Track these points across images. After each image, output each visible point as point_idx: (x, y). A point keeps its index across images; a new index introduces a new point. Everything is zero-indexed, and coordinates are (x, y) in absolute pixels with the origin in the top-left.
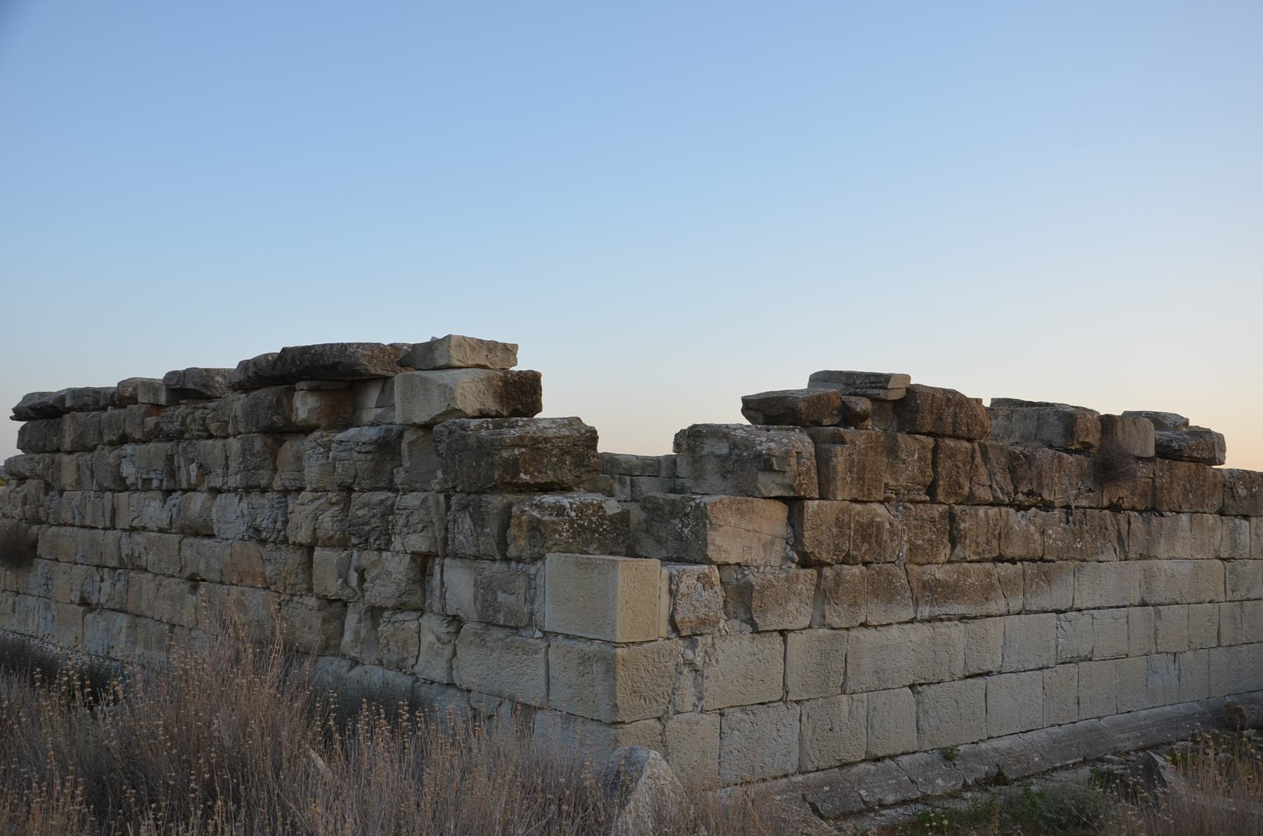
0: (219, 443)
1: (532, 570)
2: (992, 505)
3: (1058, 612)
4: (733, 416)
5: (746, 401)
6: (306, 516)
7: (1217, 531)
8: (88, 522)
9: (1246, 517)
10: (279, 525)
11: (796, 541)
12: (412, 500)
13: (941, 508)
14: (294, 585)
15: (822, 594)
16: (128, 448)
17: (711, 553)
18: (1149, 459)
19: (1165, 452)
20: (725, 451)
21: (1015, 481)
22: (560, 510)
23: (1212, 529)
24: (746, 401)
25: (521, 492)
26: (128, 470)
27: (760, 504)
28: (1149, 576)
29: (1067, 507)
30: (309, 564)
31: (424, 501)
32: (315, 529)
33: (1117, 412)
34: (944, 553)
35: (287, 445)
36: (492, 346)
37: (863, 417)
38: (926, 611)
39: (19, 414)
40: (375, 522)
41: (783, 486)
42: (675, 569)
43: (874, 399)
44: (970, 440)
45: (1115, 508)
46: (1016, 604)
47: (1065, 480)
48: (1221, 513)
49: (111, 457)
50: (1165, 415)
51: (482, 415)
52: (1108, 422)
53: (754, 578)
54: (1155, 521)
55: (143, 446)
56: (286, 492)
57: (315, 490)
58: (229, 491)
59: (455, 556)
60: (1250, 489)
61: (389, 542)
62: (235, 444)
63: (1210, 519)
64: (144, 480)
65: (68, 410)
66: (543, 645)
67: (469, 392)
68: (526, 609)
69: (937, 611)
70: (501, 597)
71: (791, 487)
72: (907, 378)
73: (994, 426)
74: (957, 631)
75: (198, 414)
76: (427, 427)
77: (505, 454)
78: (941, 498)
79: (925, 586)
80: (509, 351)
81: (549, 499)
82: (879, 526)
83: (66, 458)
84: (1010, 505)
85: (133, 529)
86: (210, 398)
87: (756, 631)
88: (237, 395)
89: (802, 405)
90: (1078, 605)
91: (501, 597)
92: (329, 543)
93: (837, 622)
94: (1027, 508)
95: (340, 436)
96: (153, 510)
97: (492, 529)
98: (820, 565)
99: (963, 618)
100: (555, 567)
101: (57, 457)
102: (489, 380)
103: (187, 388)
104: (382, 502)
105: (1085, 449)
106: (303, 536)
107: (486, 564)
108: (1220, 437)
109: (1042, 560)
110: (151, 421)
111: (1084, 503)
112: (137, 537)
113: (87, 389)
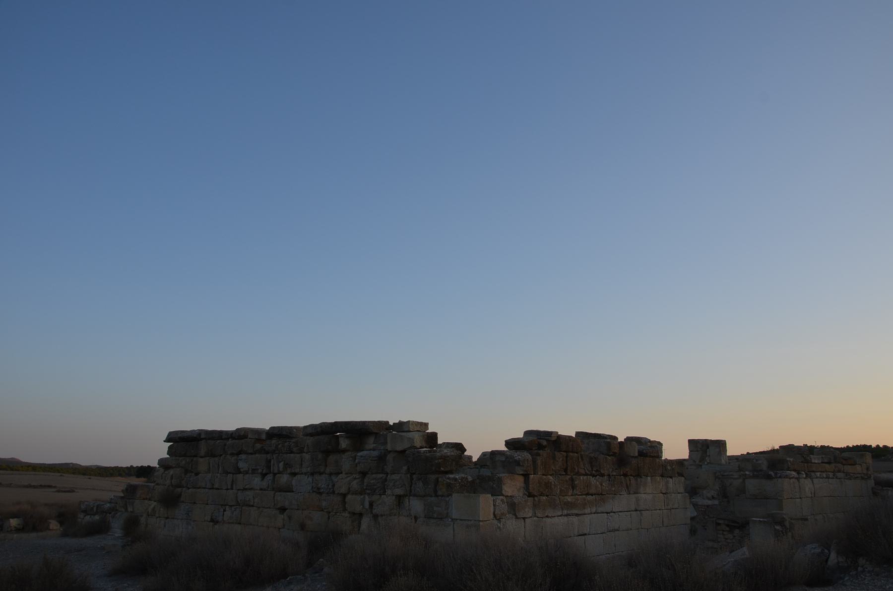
0: (298, 455)
4: (502, 447)
6: (342, 483)
8: (216, 486)
9: (671, 477)
11: (527, 487)
12: (395, 477)
15: (535, 506)
16: (243, 456)
17: (503, 492)
22: (456, 479)
27: (517, 476)
30: (344, 502)
34: (570, 492)
37: (545, 447)
38: (565, 512)
39: (167, 440)
43: (547, 440)
45: (625, 475)
46: (594, 510)
48: (662, 476)
53: (516, 501)
56: (331, 474)
59: (415, 495)
62: (307, 457)
63: (658, 478)
67: (418, 439)
70: (435, 509)
74: (575, 519)
75: (286, 444)
76: (403, 452)
80: (426, 425)
81: (451, 476)
83: (201, 460)
85: (245, 489)
86: (292, 438)
87: (517, 518)
91: (435, 509)
92: (355, 493)
93: (539, 515)
95: (360, 454)
96: (256, 481)
98: (534, 496)
100: (456, 499)
101: (195, 459)
103: (280, 434)
105: (614, 454)
106: (343, 490)
108: (660, 444)
110: (258, 446)
112: (248, 493)
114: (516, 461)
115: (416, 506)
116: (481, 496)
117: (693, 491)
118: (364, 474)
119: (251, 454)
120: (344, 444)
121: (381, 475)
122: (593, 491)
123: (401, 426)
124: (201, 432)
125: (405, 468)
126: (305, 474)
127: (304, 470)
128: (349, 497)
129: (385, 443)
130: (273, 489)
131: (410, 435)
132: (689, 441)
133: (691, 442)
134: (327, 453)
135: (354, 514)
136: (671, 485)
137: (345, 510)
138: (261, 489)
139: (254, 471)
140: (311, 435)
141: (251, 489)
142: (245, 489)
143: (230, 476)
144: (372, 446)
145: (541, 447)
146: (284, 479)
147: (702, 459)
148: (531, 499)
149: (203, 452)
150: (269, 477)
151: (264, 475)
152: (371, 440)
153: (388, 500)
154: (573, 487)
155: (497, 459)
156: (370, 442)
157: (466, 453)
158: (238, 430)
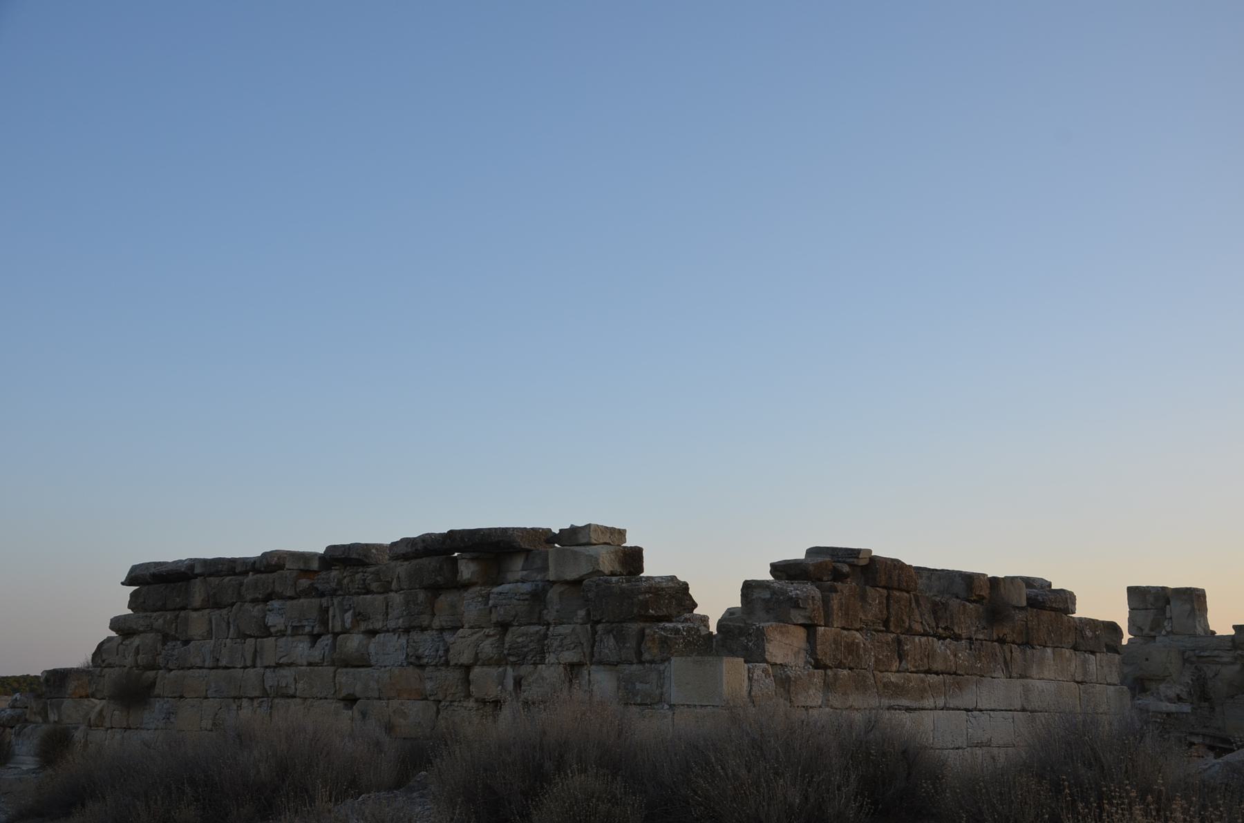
0: (381, 597)
1: (662, 667)
2: (922, 635)
3: (967, 710)
5: (772, 565)
6: (463, 646)
7: (1075, 663)
8: (223, 663)
9: (1093, 653)
10: (441, 653)
12: (564, 629)
13: (892, 636)
14: (454, 694)
15: (828, 686)
16: (276, 604)
18: (1022, 608)
19: (1033, 603)
20: (768, 596)
21: (937, 620)
22: (677, 631)
23: (1069, 660)
24: (772, 565)
25: (646, 621)
26: (271, 620)
27: (792, 627)
28: (1027, 690)
29: (970, 638)
30: (467, 682)
31: (573, 630)
32: (477, 654)
33: (1001, 575)
34: (894, 667)
35: (442, 597)
36: (612, 531)
39: (129, 582)
40: (532, 646)
41: (805, 617)
42: (750, 665)
43: (851, 565)
44: (908, 592)
45: (1002, 641)
46: (941, 703)
47: (968, 622)
49: (256, 610)
50: (1034, 580)
51: (613, 574)
52: (994, 581)
54: (1029, 651)
55: (295, 602)
56: (442, 630)
57: (471, 628)
58: (388, 631)
59: (600, 663)
60: (1094, 632)
61: (543, 658)
62: (397, 598)
63: (1067, 653)
64: (294, 627)
65: (196, 576)
66: (670, 713)
67: (607, 561)
68: (657, 692)
69: (893, 702)
70: (638, 686)
71: (810, 618)
72: (870, 551)
73: (921, 582)
75: (358, 576)
76: (578, 582)
77: (641, 597)
78: (892, 629)
79: (886, 686)
80: (621, 533)
82: (858, 644)
83: (195, 615)
84: (934, 636)
85: (279, 665)
88: (399, 563)
89: (811, 568)
90: (980, 706)
91: (638, 686)
92: (488, 663)
93: (837, 704)
94: (944, 639)
95: (496, 590)
96: (301, 649)
97: (631, 644)
98: (825, 667)
99: (908, 709)
100: (677, 665)
101: (182, 613)
102: (616, 552)
103: (346, 559)
104: (537, 632)
105: (980, 599)
106: (465, 659)
107: (626, 666)
109: (955, 673)
110: (304, 583)
111: (981, 637)
112: (285, 672)
113: (220, 559)
114: (791, 598)
115: (603, 682)
116: (725, 659)
117: (1139, 685)
118: (504, 626)
119: (291, 598)
120: (467, 570)
121: (537, 628)
122: (938, 666)
123: (572, 536)
124: (193, 563)
125: (582, 613)
126: (394, 631)
127: (392, 624)
128: (476, 670)
129: (545, 568)
130: (333, 664)
131: (591, 550)
132: (1130, 590)
133: (1133, 592)
134: (435, 590)
135: (484, 702)
136: (1092, 667)
137: (468, 696)
138: (310, 664)
139: (296, 631)
140: (405, 557)
141: (290, 665)
142: (279, 665)
143: (250, 641)
144: (519, 575)
145: (838, 576)
146: (354, 642)
147: (1156, 625)
148: (821, 671)
149: (197, 600)
150: (326, 640)
151: (315, 638)
152: (518, 563)
153: (551, 672)
154: (901, 657)
155: (755, 595)
156: (517, 567)
157: (696, 611)
158: (264, 554)
